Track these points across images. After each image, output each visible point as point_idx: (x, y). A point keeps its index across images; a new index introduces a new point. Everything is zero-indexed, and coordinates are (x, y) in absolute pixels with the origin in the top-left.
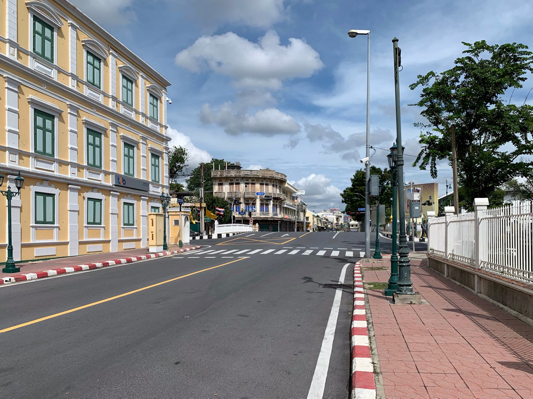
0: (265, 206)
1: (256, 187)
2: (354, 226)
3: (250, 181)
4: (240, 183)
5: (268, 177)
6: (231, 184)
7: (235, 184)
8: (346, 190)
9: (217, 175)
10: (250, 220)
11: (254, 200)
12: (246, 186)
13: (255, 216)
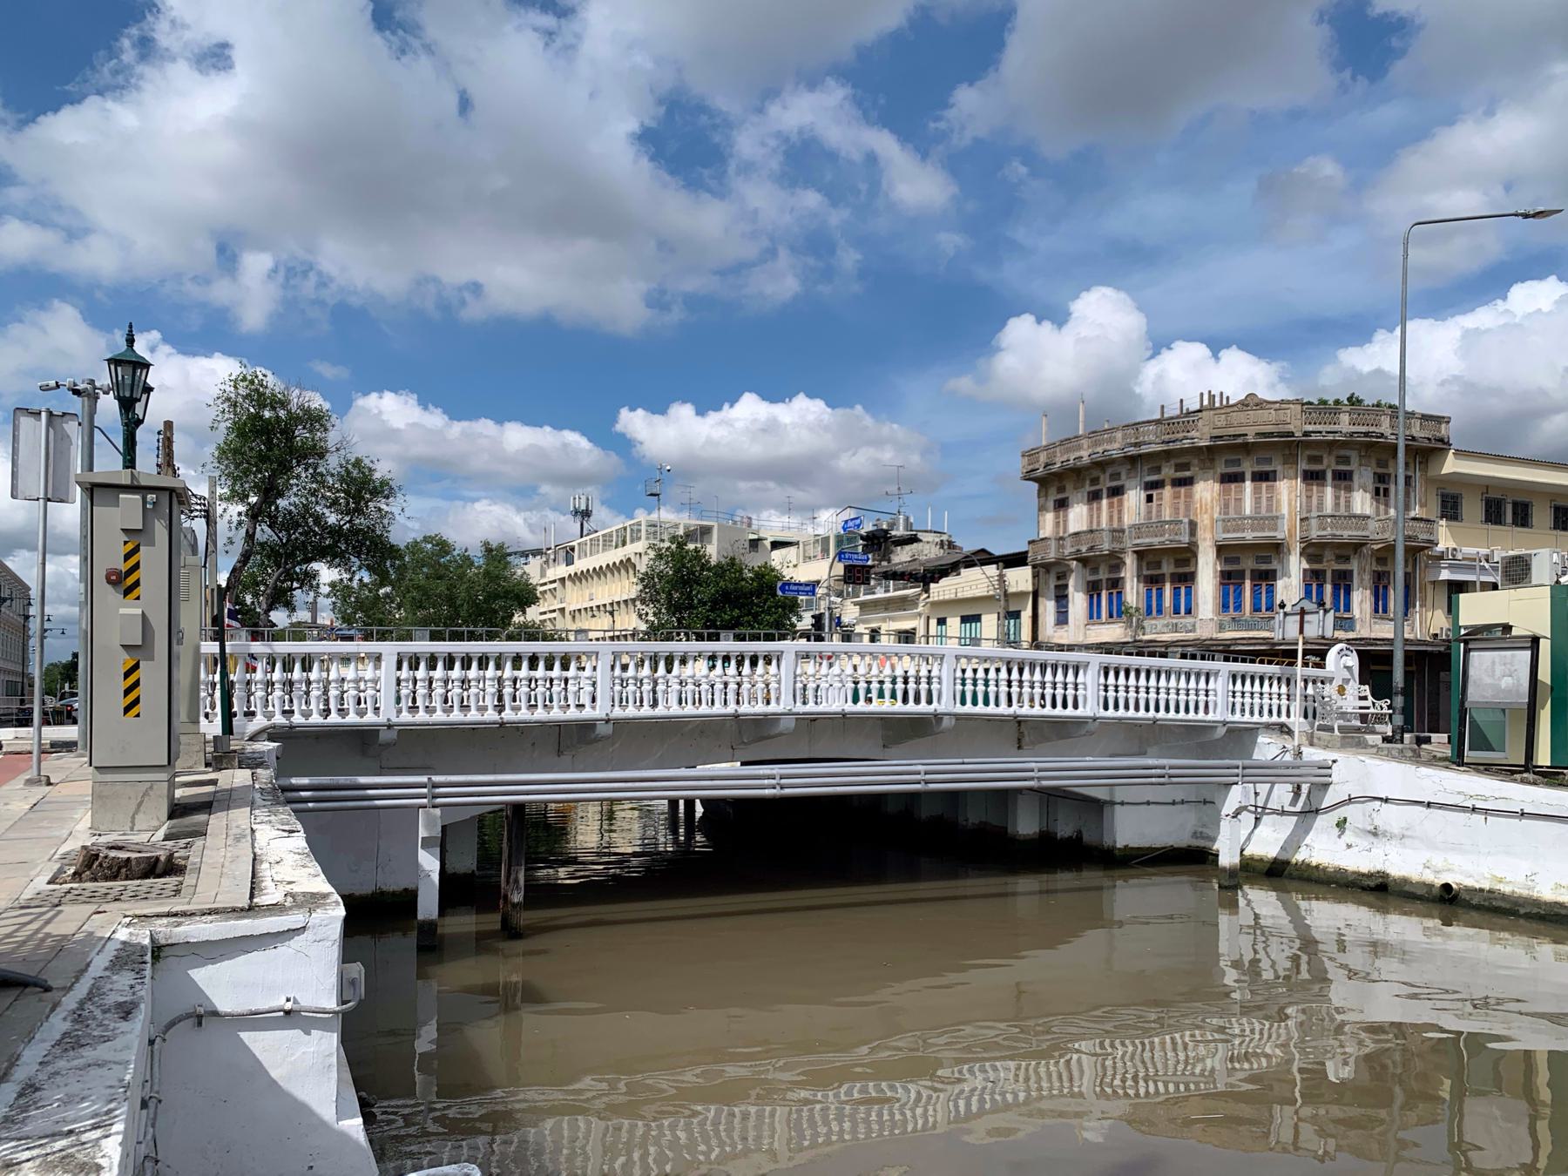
0: (1248, 584)
1: (1197, 497)
3: (1168, 472)
4: (1127, 486)
5: (1250, 439)
6: (1313, 477)
7: (1253, 480)
9: (1037, 466)
11: (1185, 556)
12: (1149, 499)
13: (1191, 636)
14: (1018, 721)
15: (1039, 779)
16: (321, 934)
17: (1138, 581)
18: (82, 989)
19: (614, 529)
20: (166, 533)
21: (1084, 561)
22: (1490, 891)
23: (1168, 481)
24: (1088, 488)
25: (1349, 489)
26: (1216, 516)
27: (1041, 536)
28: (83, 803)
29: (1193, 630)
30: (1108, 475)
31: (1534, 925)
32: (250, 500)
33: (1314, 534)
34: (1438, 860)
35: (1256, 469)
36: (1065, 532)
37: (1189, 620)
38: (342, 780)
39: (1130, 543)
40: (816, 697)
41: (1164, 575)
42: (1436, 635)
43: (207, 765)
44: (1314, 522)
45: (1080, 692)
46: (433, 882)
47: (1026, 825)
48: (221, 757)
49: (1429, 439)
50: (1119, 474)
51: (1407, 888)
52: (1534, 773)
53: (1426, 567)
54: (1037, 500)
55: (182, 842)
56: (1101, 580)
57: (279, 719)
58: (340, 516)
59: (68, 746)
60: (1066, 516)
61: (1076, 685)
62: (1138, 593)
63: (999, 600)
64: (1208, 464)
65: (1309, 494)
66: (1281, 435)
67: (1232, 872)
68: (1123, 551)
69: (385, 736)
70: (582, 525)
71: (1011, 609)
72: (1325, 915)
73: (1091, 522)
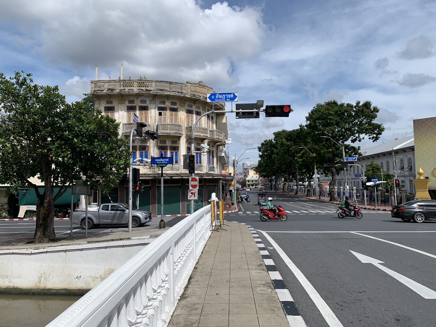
1: (179, 117)
2: (250, 181)
3: (168, 104)
6: (131, 109)
7: (140, 110)
8: (264, 142)
10: (191, 183)
12: (160, 114)
41: (167, 146)
56: (136, 146)
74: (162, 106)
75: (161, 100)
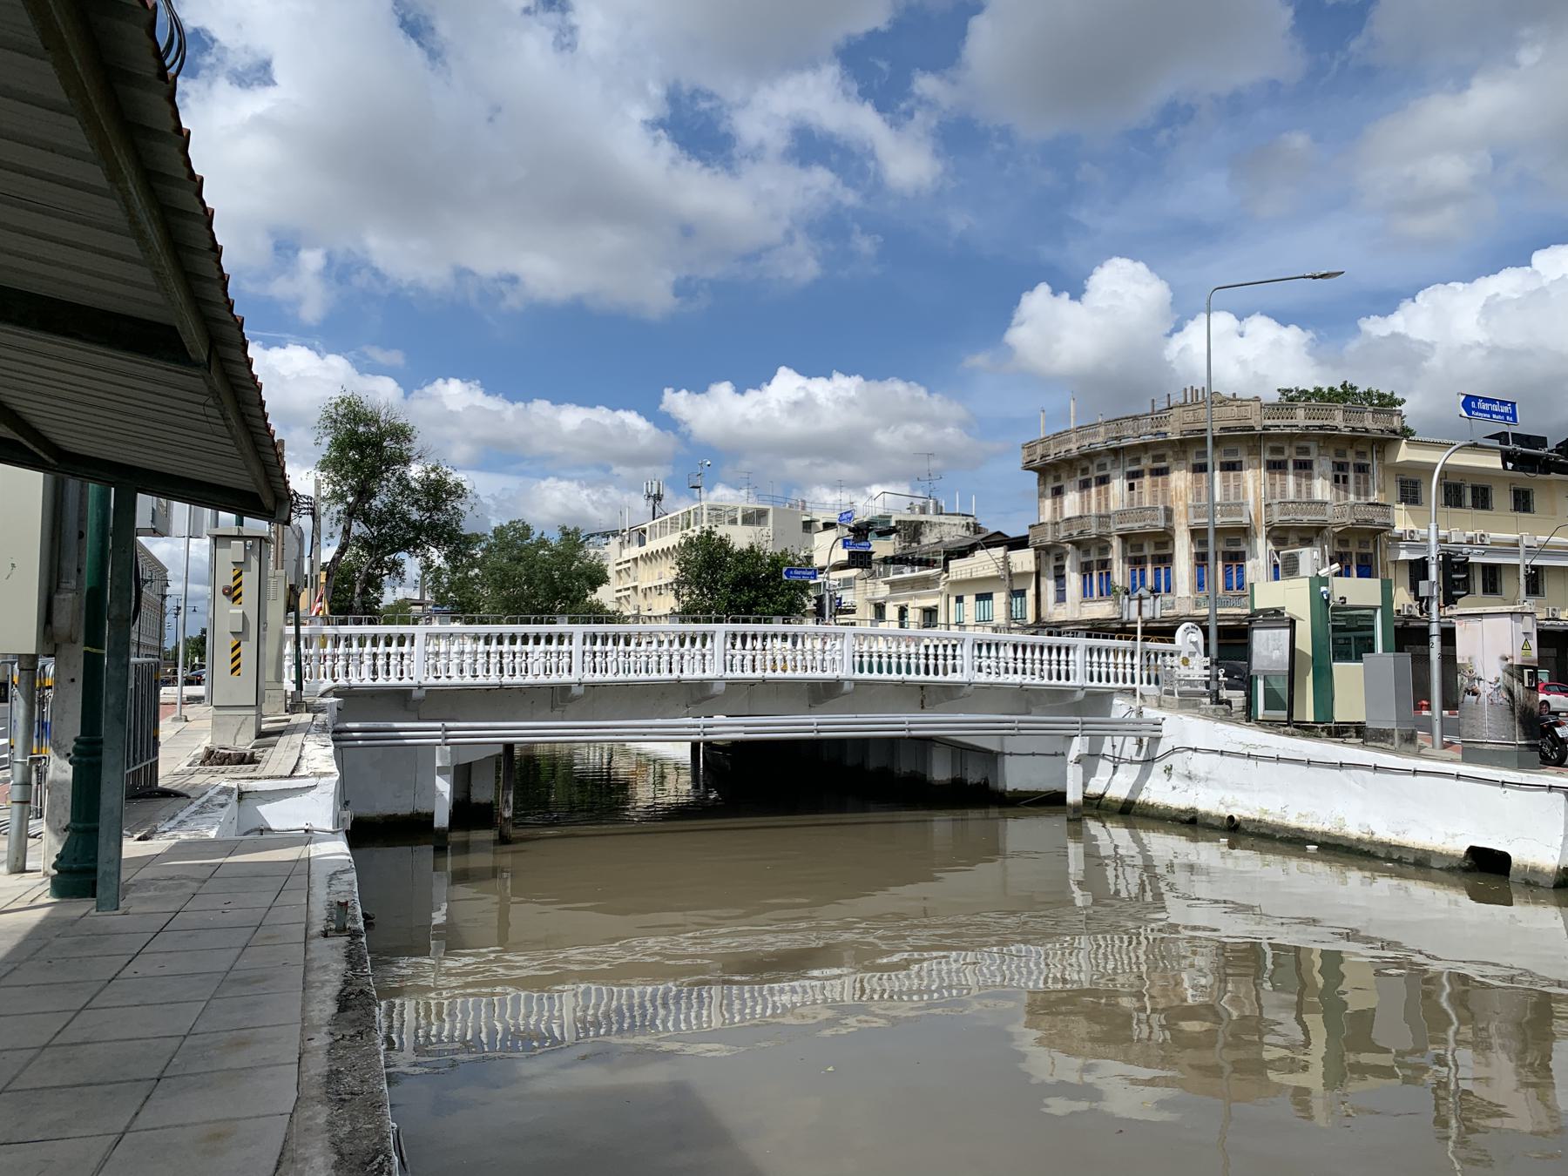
1: (1172, 485)
3: (1147, 463)
4: (1112, 476)
6: (1276, 467)
7: (1221, 470)
11: (1164, 539)
12: (1131, 487)
14: (922, 687)
15: (910, 730)
16: (325, 789)
17: (1123, 562)
18: (204, 799)
19: (679, 512)
20: (258, 563)
21: (1077, 544)
22: (1259, 821)
23: (1147, 471)
24: (1080, 477)
25: (1310, 477)
26: (1190, 502)
27: (1041, 521)
28: (207, 731)
29: (1173, 607)
30: (1095, 465)
31: (1284, 847)
32: (348, 499)
33: (1276, 519)
34: (1229, 799)
35: (1224, 460)
36: (1061, 517)
37: (1168, 598)
38: (382, 725)
39: (1114, 527)
40: (743, 666)
42: (1399, 611)
43: (286, 711)
44: (1276, 508)
45: (1071, 667)
46: (445, 799)
47: (940, 772)
48: (296, 705)
49: (1382, 431)
50: (1105, 464)
51: (1209, 821)
52: (1295, 727)
53: (1387, 547)
54: (1037, 487)
55: (261, 750)
57: (342, 681)
58: (421, 513)
59: (198, 699)
60: (1062, 503)
61: (1067, 662)
62: (1123, 573)
63: (1004, 580)
64: (1181, 455)
65: (1272, 482)
66: (1243, 429)
67: (1076, 808)
68: (1109, 535)
69: (417, 694)
70: (654, 508)
71: (1015, 588)
72: (1163, 845)
73: (1083, 508)
74: (1135, 468)
75: (1132, 457)
